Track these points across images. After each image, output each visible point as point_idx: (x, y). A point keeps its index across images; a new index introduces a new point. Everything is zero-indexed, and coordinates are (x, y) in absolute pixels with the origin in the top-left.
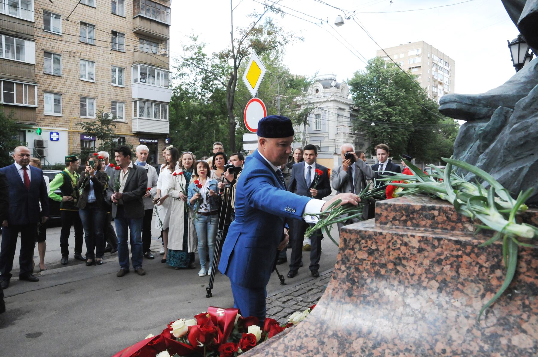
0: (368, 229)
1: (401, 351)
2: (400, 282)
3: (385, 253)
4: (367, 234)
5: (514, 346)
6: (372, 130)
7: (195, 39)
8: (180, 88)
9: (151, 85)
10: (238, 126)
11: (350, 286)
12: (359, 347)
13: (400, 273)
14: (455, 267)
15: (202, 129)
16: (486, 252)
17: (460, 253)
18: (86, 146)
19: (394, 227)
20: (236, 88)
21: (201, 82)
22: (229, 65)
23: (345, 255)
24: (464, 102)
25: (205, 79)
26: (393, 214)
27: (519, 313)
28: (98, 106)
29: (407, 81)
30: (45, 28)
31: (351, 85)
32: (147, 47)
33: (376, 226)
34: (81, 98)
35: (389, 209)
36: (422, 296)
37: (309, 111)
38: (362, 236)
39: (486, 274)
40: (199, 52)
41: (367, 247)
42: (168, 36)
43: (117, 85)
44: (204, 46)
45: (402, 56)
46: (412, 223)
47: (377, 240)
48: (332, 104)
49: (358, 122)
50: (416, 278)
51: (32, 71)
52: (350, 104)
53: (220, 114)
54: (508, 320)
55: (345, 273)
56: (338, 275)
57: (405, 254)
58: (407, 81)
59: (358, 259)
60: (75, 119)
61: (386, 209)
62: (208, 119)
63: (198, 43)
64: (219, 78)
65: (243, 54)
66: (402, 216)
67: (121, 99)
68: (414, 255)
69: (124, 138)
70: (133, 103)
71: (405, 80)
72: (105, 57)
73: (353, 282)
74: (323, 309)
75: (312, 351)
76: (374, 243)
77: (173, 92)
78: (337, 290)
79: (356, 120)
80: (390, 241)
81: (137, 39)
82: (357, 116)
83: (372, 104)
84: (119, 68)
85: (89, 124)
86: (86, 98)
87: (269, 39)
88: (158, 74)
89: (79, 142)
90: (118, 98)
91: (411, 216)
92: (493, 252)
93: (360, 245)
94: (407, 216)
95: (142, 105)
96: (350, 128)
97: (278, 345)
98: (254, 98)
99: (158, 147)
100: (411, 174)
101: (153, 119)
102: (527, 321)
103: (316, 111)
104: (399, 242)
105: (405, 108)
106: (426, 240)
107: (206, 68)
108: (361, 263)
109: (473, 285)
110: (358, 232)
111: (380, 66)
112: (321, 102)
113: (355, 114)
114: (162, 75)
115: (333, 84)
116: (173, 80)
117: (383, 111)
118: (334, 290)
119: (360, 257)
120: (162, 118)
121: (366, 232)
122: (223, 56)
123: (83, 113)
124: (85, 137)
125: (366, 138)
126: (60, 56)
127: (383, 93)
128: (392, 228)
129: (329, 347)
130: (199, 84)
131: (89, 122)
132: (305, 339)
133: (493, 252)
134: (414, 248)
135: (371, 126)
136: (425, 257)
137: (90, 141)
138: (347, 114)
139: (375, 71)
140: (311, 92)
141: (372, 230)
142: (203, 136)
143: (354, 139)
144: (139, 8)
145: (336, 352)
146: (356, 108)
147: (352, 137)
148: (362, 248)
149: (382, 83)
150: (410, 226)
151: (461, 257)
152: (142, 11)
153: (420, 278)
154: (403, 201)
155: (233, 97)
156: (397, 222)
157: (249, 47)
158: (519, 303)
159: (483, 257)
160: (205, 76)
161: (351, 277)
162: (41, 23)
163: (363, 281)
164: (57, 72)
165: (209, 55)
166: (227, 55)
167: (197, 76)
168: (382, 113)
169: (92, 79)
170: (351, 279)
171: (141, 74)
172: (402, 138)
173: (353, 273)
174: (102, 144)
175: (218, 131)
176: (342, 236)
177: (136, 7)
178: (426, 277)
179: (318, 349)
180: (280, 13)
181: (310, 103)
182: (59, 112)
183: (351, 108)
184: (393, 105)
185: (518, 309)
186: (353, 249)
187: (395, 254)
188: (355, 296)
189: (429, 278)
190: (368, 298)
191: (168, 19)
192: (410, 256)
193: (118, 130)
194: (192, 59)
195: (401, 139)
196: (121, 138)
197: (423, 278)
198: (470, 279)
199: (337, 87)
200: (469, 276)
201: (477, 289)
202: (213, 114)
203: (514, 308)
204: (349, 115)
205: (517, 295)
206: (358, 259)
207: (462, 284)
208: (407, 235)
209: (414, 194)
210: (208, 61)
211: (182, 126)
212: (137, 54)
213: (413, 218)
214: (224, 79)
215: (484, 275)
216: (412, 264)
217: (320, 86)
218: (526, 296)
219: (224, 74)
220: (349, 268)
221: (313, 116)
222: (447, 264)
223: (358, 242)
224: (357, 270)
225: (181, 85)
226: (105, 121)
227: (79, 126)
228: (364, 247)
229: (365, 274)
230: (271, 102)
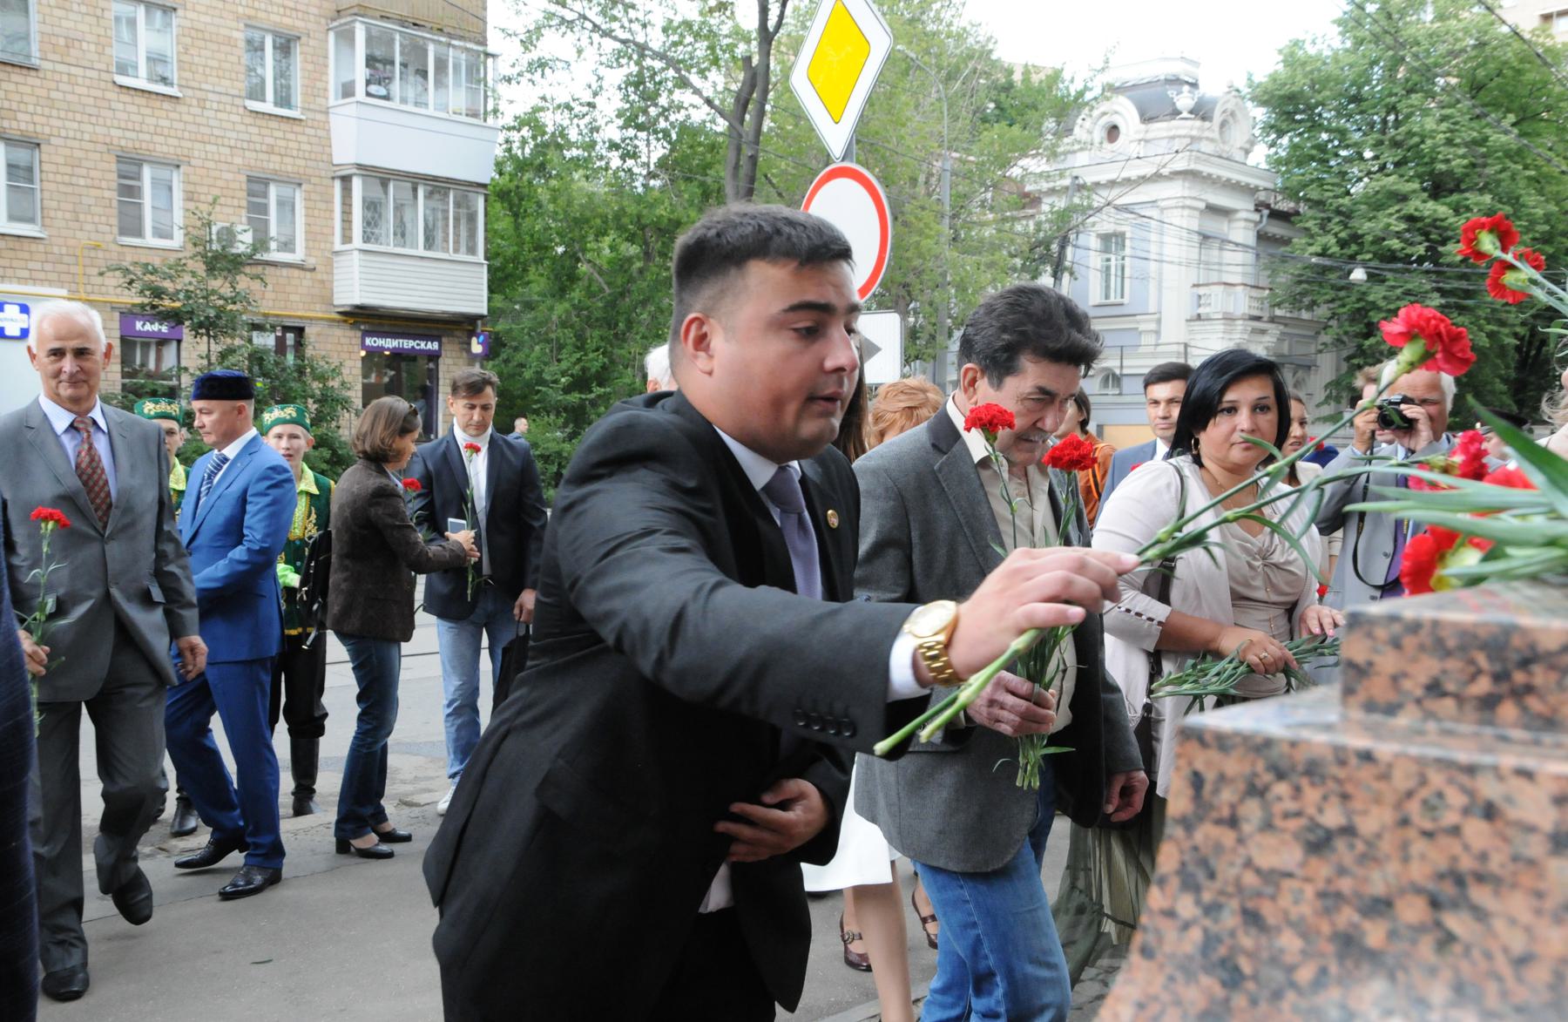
0: (1305, 734)
2: (1459, 988)
3: (1386, 846)
4: (1301, 756)
6: (1352, 303)
8: (530, 121)
9: (410, 108)
11: (1219, 992)
13: (1457, 948)
15: (622, 295)
18: (143, 365)
19: (1431, 726)
20: (767, 124)
21: (620, 95)
22: (737, 26)
23: (1196, 848)
25: (637, 82)
26: (1428, 667)
28: (190, 197)
29: (1530, 76)
31: (1264, 103)
33: (1345, 718)
34: (120, 159)
35: (1409, 642)
37: (1077, 219)
41: (1298, 814)
43: (268, 107)
46: (1524, 709)
47: (1349, 788)
48: (1176, 189)
49: (1294, 269)
52: (1256, 189)
55: (1196, 935)
56: (1160, 939)
57: (1483, 857)
58: (1530, 76)
59: (1258, 871)
60: (96, 248)
61: (1396, 644)
62: (647, 255)
64: (694, 78)
66: (1473, 678)
67: (289, 166)
68: (1531, 863)
69: (299, 331)
70: (338, 184)
71: (1519, 72)
73: (1233, 978)
76: (1334, 800)
77: (501, 137)
78: (1154, 1008)
79: (1284, 259)
80: (1409, 794)
82: (1286, 242)
83: (1356, 190)
84: (276, 34)
85: (155, 271)
86: (139, 163)
88: (441, 65)
90: (274, 163)
91: (1519, 677)
93: (1266, 807)
94: (1498, 678)
95: (377, 192)
96: (1255, 293)
99: (442, 368)
100: (1526, 485)
101: (421, 251)
103: (1106, 223)
104: (1456, 799)
105: (1515, 201)
107: (640, 39)
108: (1269, 890)
110: (1261, 746)
111: (1403, 13)
112: (1128, 181)
113: (1277, 229)
114: (457, 67)
115: (1185, 101)
116: (502, 88)
117: (1410, 219)
118: (1141, 1006)
119: (1265, 861)
120: (456, 250)
121: (1293, 744)
124: (139, 325)
125: (1326, 338)
127: (1410, 134)
128: (1420, 733)
130: (611, 104)
131: (157, 262)
134: (1531, 829)
135: (1350, 287)
137: (162, 342)
138: (1242, 231)
139: (1376, 39)
141: (1321, 738)
142: (629, 324)
146: (1286, 205)
147: (1263, 332)
148: (1278, 822)
149: (1410, 91)
150: (1515, 726)
154: (1478, 609)
155: (753, 159)
156: (1448, 704)
160: (634, 69)
161: (1222, 951)
163: (1278, 976)
164: (17, 47)
167: (603, 71)
168: (1403, 226)
169: (164, 80)
170: (1223, 962)
171: (371, 61)
172: (1491, 335)
173: (1232, 934)
174: (208, 357)
176: (1182, 762)
182: (32, 220)
183: (1259, 207)
184: (1457, 189)
186: (1233, 822)
192: (1511, 867)
193: (274, 298)
195: (1484, 341)
196: (286, 329)
199: (1201, 112)
204: (1249, 238)
206: (1258, 871)
208: (1495, 769)
209: (1534, 579)
211: (538, 282)
213: (1529, 689)
217: (1125, 112)
219: (715, 62)
220: (1212, 910)
221: (1094, 243)
223: (1255, 790)
224: (1252, 918)
225: (536, 110)
226: (223, 262)
228: (1287, 816)
229: (1289, 942)
230: (914, 181)
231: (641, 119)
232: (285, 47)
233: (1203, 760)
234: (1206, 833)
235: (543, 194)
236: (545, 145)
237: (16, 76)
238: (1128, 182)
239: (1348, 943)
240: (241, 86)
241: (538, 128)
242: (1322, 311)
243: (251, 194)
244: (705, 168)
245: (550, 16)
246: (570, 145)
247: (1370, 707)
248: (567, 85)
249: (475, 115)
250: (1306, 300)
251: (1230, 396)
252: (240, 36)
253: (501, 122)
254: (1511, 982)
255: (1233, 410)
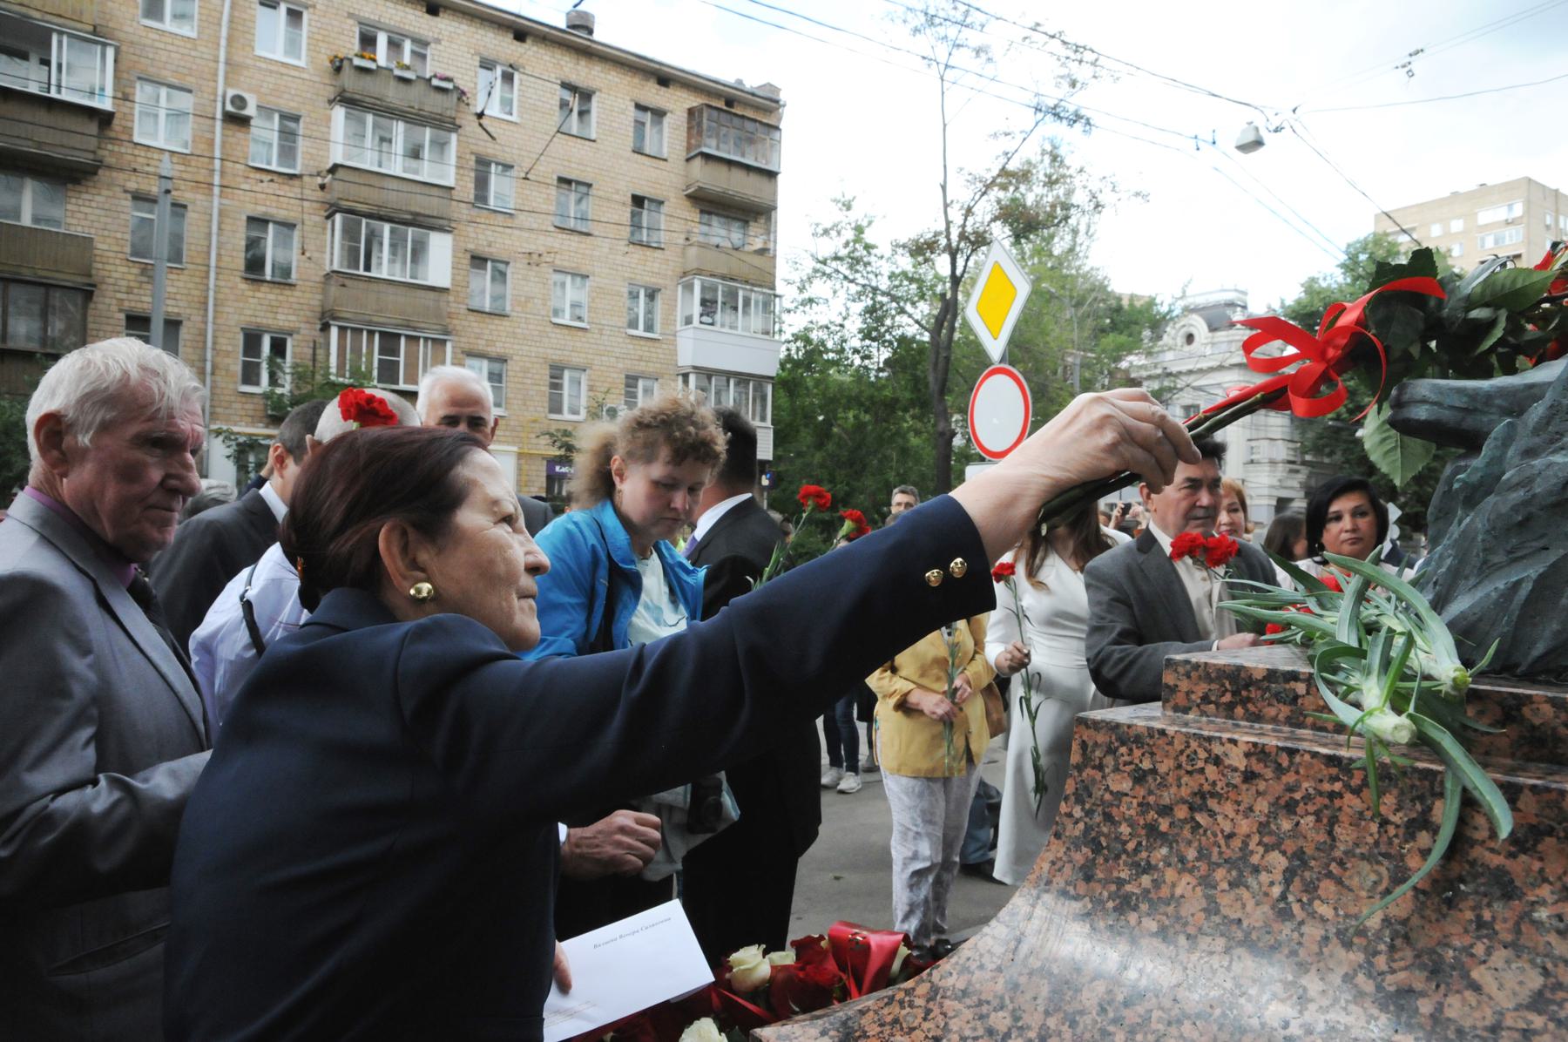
0: (1135, 721)
1: (1188, 1018)
3: (1170, 779)
4: (1132, 732)
5: (1449, 1019)
7: (848, 206)
8: (803, 337)
10: (958, 441)
12: (1095, 1001)
14: (1325, 821)
16: (1396, 786)
17: (1337, 786)
19: (1204, 719)
20: (957, 335)
21: (860, 319)
24: (1447, 401)
25: (871, 311)
26: (1201, 689)
27: (1467, 940)
28: (591, 388)
30: (477, 198)
32: (721, 233)
34: (552, 367)
36: (1247, 888)
38: (1123, 736)
39: (1396, 841)
40: (857, 240)
42: (775, 201)
43: (640, 332)
44: (870, 223)
45: (1457, 226)
50: (1236, 843)
51: (443, 305)
53: (912, 403)
54: (1440, 955)
55: (1081, 826)
57: (1214, 784)
62: (877, 421)
63: (856, 215)
64: (908, 308)
65: (979, 240)
67: (650, 368)
68: (1235, 787)
70: (680, 379)
72: (612, 260)
73: (1097, 848)
74: (1026, 909)
75: (988, 1003)
78: (1060, 864)
80: (1182, 752)
81: (696, 216)
86: (562, 369)
87: (1050, 199)
88: (747, 302)
89: (543, 481)
90: (642, 367)
91: (1244, 693)
92: (1413, 786)
93: (1116, 760)
94: (1234, 694)
95: (705, 383)
96: (1291, 445)
97: (917, 983)
98: (997, 366)
102: (1485, 962)
104: (1203, 755)
106: (1263, 751)
107: (874, 284)
109: (1365, 866)
110: (1114, 727)
114: (757, 303)
116: (785, 317)
118: (1053, 863)
119: (1114, 788)
121: (1129, 726)
122: (922, 250)
123: (556, 407)
124: (557, 469)
126: (507, 263)
129: (1028, 996)
130: (855, 324)
132: (978, 974)
133: (1413, 786)
134: (1235, 770)
136: (1259, 793)
140: (1171, 342)
141: (1141, 723)
142: (864, 467)
143: (1302, 477)
144: (700, 133)
145: (1041, 1009)
147: (1297, 471)
151: (1341, 795)
152: (708, 141)
153: (1245, 844)
155: (947, 359)
156: (1212, 706)
157: (994, 219)
158: (1469, 915)
159: (1390, 800)
160: (870, 303)
161: (1093, 834)
162: (468, 190)
164: (499, 303)
165: (884, 249)
166: (931, 246)
167: (850, 304)
169: (580, 319)
171: (704, 302)
175: (905, 452)
177: (695, 131)
178: (1259, 844)
179: (1002, 998)
180: (1079, 126)
181: (1170, 374)
185: (1466, 931)
186: (1100, 767)
187: (1191, 783)
188: (1099, 881)
189: (1266, 845)
190: (1128, 888)
191: (775, 155)
194: (837, 258)
197: (1252, 846)
198: (1358, 851)
200: (1357, 845)
201: (1373, 877)
202: (891, 406)
203: (1455, 929)
205: (1465, 895)
207: (1341, 863)
210: (881, 262)
211: (806, 437)
212: (693, 251)
213: (1249, 700)
214: (924, 309)
215: (1390, 843)
216: (1228, 808)
217: (1199, 326)
218: (1485, 901)
219: (922, 297)
220: (1089, 813)
222: (1307, 813)
223: (1111, 751)
224: (1108, 817)
227: (545, 440)
229: (1125, 829)
231: (874, 334)
232: (652, 295)
233: (1087, 735)
234: (1088, 772)
235: (810, 383)
236: (812, 351)
237: (497, 321)
238: (1201, 371)
239: (1152, 829)
240: (624, 321)
241: (808, 341)
242: (1338, 457)
243: (627, 385)
244: (915, 364)
245: (816, 271)
246: (827, 351)
247: (1176, 709)
248: (823, 315)
249: (767, 333)
250: (1327, 450)
251: (1334, 508)
252: (625, 290)
253: (784, 338)
254: (1224, 849)
255: (1338, 518)
